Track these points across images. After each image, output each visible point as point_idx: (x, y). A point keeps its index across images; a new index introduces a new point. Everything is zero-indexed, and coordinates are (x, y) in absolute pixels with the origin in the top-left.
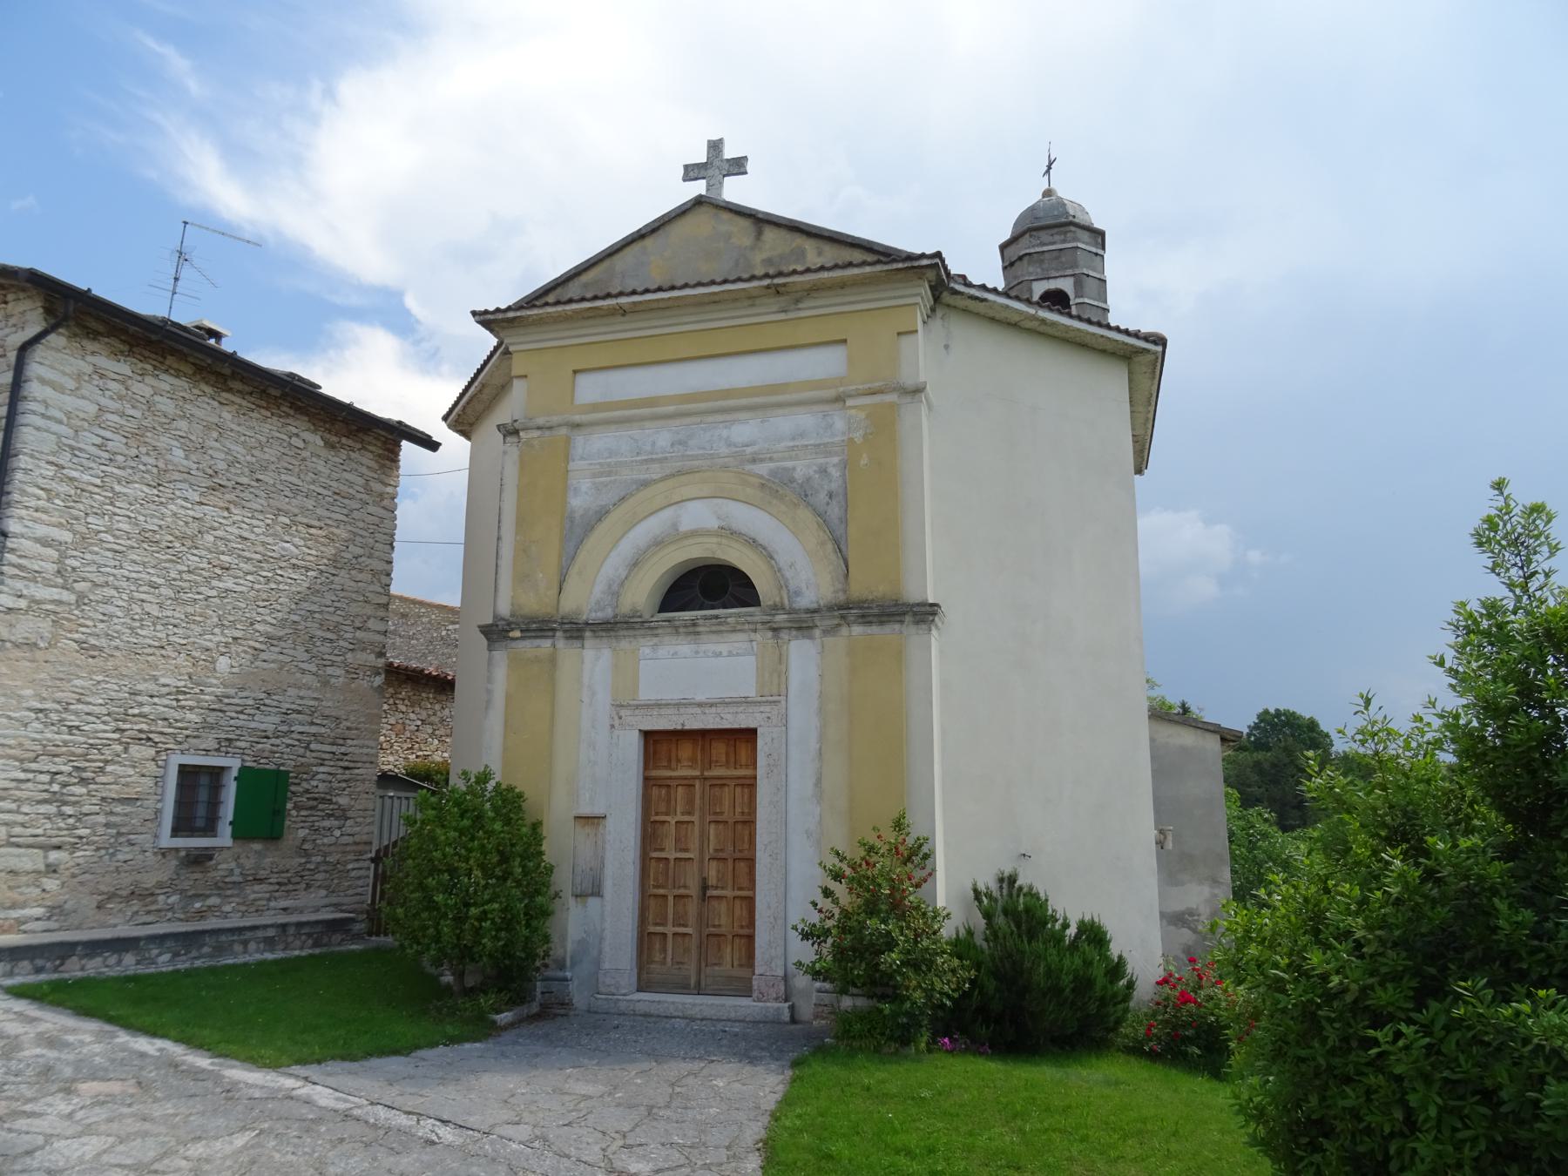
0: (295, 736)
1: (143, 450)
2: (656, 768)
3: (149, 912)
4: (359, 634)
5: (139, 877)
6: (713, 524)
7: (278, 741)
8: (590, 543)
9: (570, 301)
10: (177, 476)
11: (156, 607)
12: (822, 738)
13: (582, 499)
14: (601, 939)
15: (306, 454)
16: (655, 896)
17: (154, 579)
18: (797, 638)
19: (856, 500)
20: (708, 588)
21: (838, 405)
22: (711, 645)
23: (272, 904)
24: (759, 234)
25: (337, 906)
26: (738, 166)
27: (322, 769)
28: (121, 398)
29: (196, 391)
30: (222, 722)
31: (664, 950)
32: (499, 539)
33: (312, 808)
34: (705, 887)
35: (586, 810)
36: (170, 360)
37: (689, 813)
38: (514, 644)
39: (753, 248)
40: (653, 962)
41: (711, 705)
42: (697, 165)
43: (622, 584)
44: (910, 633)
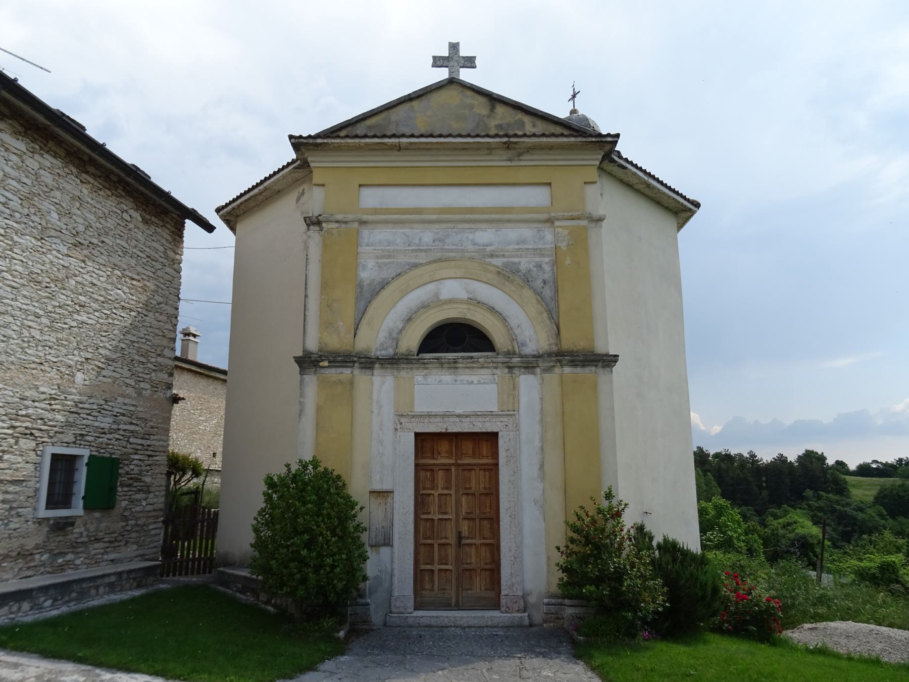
0: (121, 432)
1: (32, 211)
2: (423, 458)
3: (29, 568)
4: (159, 359)
5: (23, 541)
6: (464, 295)
7: (110, 436)
8: (376, 303)
9: (356, 136)
10: (53, 233)
11: (38, 332)
12: (543, 440)
13: (369, 272)
14: (392, 576)
15: (131, 226)
16: (424, 544)
17: (38, 311)
18: (524, 374)
19: (562, 285)
20: (456, 339)
21: (549, 224)
22: (465, 376)
23: (105, 557)
24: (493, 108)
25: (143, 557)
26: (470, 62)
27: (136, 457)
28: (19, 168)
29: (66, 170)
30: (78, 422)
31: (432, 581)
32: (306, 296)
33: (129, 485)
34: (460, 538)
35: (377, 487)
36: (51, 144)
37: (447, 488)
38: (322, 371)
39: (489, 116)
40: (424, 589)
41: (467, 416)
42: (442, 57)
43: (400, 332)
44: (602, 376)
